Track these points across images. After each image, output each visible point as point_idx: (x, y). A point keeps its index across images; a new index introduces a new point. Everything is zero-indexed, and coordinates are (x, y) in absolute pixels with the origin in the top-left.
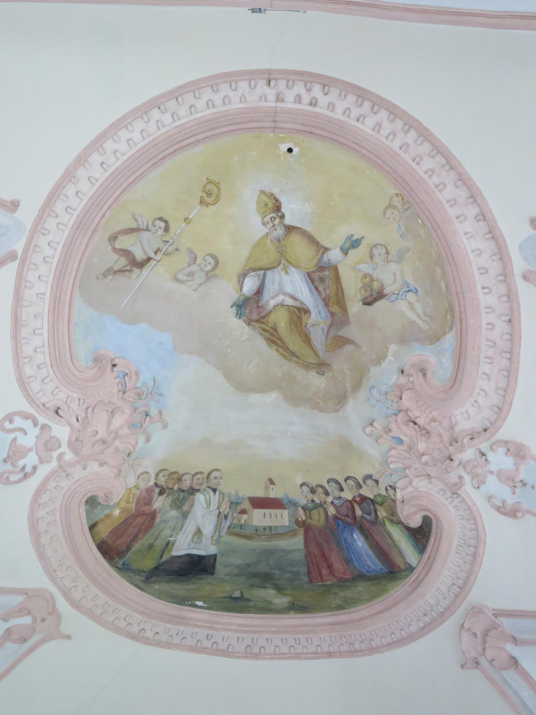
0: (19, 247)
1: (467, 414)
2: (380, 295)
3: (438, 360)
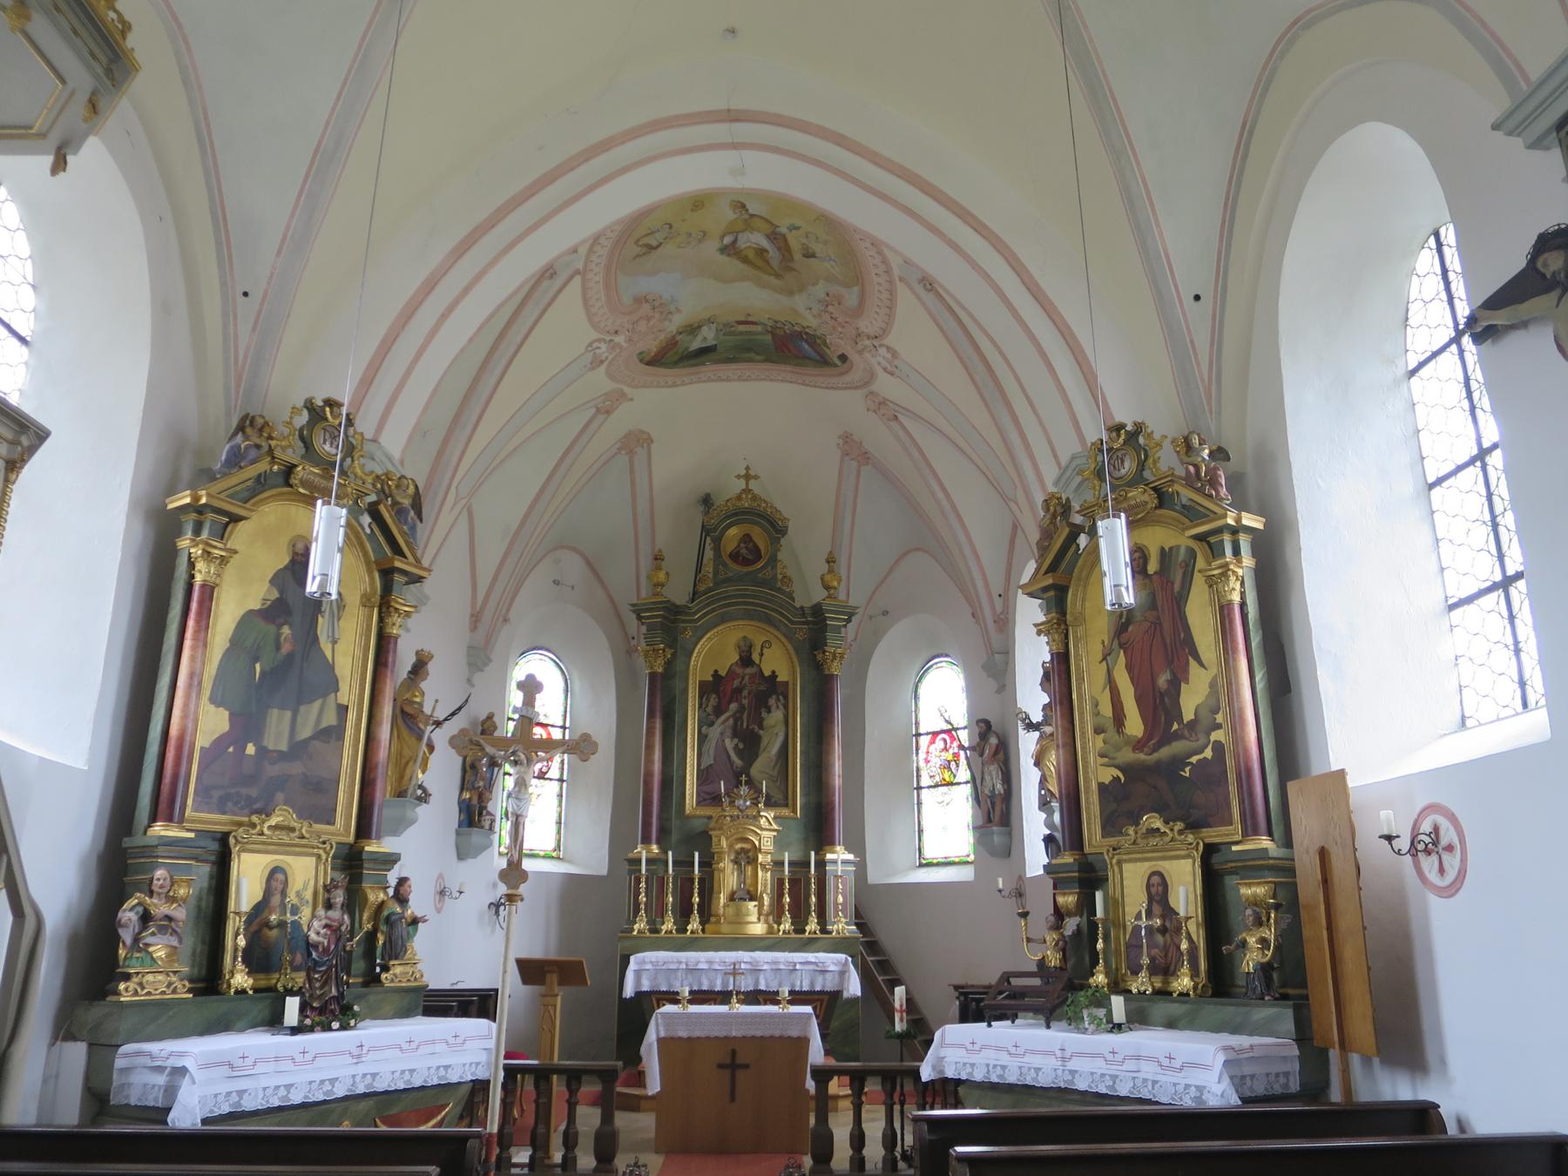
0: (580, 266)
1: (867, 325)
2: (813, 256)
3: (851, 297)
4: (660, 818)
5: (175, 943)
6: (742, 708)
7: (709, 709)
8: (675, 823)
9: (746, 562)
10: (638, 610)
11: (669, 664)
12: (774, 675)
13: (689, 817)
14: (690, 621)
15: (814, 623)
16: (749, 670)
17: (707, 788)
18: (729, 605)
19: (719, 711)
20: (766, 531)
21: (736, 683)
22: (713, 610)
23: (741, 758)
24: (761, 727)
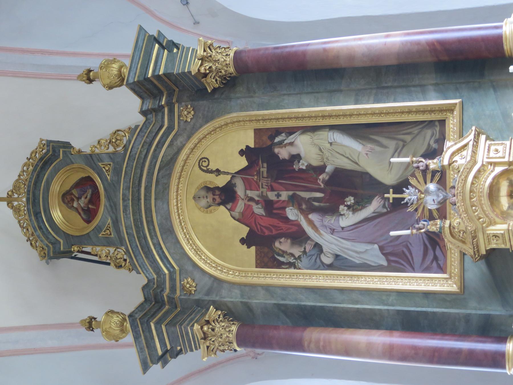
4: (464, 335)
5: (445, 194)
6: (294, 200)
7: (297, 251)
8: (475, 309)
9: (95, 199)
10: (149, 359)
11: (230, 314)
12: (246, 152)
13: (463, 286)
14: (172, 279)
15: (170, 95)
16: (240, 189)
17: (417, 252)
18: (150, 222)
19: (299, 237)
20: (56, 171)
21: (258, 210)
22: (158, 246)
23: (370, 202)
24: (321, 169)
